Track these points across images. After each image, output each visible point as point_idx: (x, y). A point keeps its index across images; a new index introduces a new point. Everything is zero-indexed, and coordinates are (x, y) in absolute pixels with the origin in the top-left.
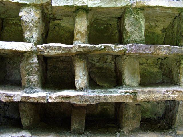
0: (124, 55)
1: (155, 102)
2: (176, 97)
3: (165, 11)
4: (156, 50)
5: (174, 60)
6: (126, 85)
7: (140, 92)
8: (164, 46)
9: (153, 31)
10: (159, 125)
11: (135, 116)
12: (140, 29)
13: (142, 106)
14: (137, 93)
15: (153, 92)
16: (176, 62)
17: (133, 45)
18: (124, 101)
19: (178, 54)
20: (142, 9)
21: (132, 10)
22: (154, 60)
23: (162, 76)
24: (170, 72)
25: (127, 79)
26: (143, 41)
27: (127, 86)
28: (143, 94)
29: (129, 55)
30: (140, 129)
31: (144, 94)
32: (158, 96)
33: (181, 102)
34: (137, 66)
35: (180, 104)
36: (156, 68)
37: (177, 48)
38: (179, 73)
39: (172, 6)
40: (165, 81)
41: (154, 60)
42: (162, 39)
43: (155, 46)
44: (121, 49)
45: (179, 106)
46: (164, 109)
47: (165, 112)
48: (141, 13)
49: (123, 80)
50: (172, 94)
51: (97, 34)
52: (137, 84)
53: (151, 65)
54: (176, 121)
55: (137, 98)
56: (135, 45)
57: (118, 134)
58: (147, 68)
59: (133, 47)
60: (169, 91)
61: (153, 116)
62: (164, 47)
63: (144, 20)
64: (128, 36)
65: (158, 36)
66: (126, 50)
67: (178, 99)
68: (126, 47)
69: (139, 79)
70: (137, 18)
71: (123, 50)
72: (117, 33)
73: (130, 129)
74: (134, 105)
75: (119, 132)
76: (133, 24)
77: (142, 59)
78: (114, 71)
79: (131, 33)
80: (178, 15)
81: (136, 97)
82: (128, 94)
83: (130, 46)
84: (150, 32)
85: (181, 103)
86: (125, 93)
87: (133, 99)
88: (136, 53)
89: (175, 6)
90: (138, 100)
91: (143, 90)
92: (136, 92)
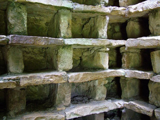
0: (8, 45)
1: (42, 86)
2: (54, 81)
3: (45, 8)
4: (36, 41)
5: (53, 49)
6: (11, 73)
7: (23, 78)
8: (43, 37)
9: (38, 24)
10: (44, 105)
11: (20, 99)
12: (23, 21)
13: (30, 90)
14: (20, 79)
15: (34, 77)
16: (55, 51)
17: (15, 36)
18: (8, 87)
19: (55, 44)
20: (24, 4)
21: (14, 4)
22: (39, 49)
23: (47, 63)
24: (52, 59)
25: (12, 68)
26: (25, 32)
27: (12, 74)
28: (25, 79)
29: (12, 45)
30: (26, 111)
31: (26, 80)
32: (38, 80)
33: (60, 84)
34: (21, 55)
35: (59, 86)
36: (41, 56)
37: (54, 40)
38: (57, 60)
39: (50, 4)
40: (49, 67)
41: (39, 49)
42: (45, 31)
43: (35, 38)
44: (4, 39)
45: (58, 88)
46: (49, 90)
47: (50, 94)
48: (24, 8)
49: (8, 69)
50: (51, 78)
51: (34, 17)
52: (21, 71)
53: (36, 54)
54: (57, 100)
55: (20, 84)
56: (17, 36)
57: (5, 118)
58: (33, 56)
59: (15, 38)
60: (48, 76)
61: (40, 98)
62: (43, 39)
63: (26, 14)
64: (11, 28)
65: (42, 29)
66: (9, 40)
67: (56, 82)
68: (9, 38)
69: (23, 67)
70: (19, 11)
71: (5, 40)
72: (4, 24)
73: (16, 111)
74: (19, 89)
75: (6, 116)
76: (15, 17)
77: (29, 48)
78: (3, 59)
79: (14, 25)
80: (56, 12)
81: (20, 83)
82: (11, 80)
83: (12, 37)
84: (36, 25)
85: (59, 84)
86: (9, 80)
87: (16, 84)
88: (18, 43)
89: (52, 5)
90: (21, 85)
91: (25, 76)
92: (19, 78)
